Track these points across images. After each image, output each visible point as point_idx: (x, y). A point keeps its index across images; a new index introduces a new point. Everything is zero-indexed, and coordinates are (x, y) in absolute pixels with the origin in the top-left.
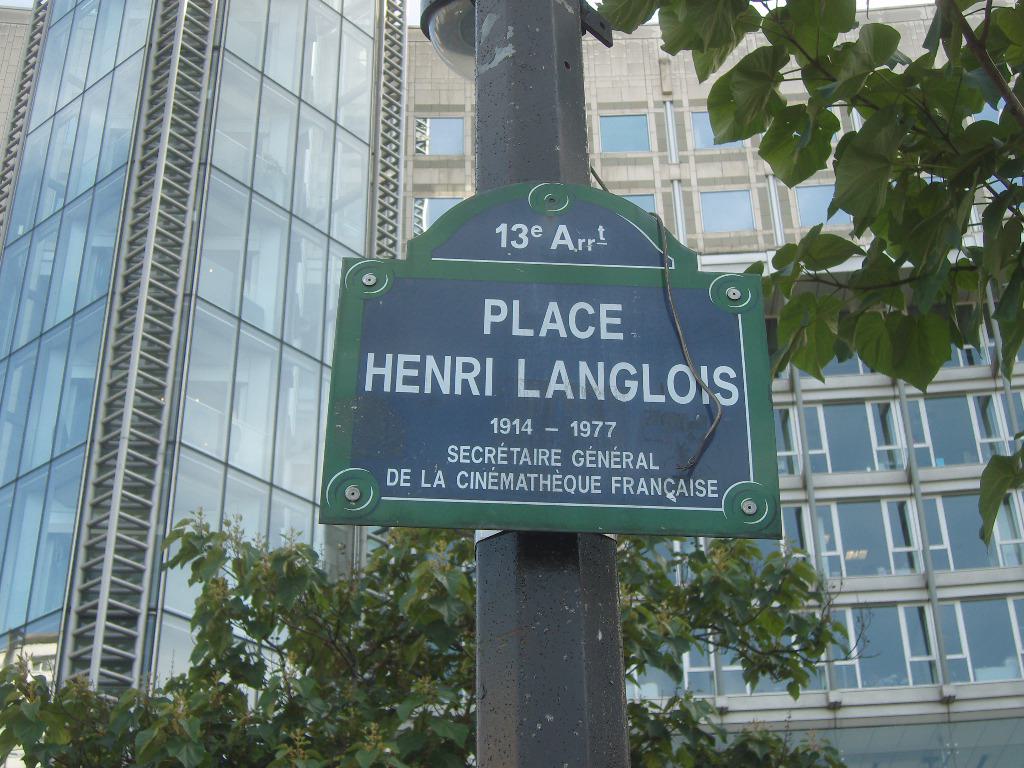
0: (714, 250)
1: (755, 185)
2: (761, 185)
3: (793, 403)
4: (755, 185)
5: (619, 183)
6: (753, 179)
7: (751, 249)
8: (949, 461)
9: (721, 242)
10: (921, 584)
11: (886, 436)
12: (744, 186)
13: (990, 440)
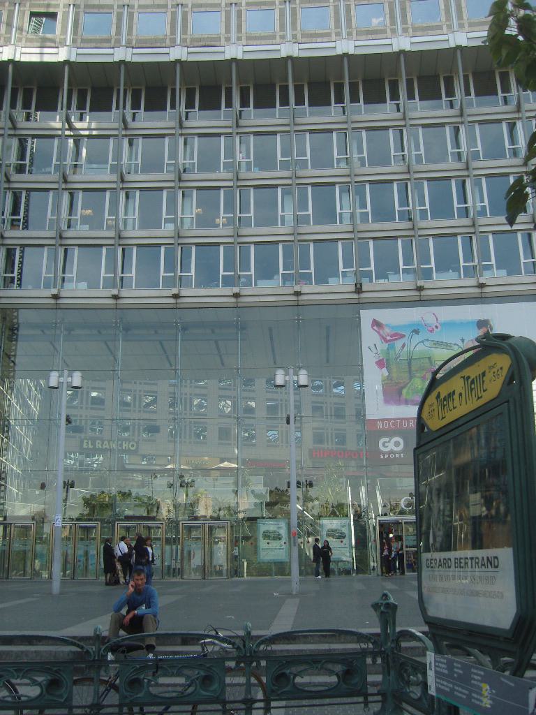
0: (140, 45)
1: (170, 10)
2: (173, 10)
3: (462, 123)
4: (170, 10)
5: (94, 5)
6: (170, 6)
7: (162, 46)
8: (262, 169)
9: (145, 41)
10: (471, 224)
11: (457, 144)
12: (163, 10)
13: (514, 147)
